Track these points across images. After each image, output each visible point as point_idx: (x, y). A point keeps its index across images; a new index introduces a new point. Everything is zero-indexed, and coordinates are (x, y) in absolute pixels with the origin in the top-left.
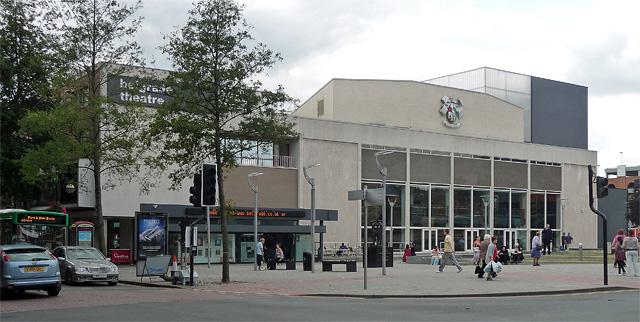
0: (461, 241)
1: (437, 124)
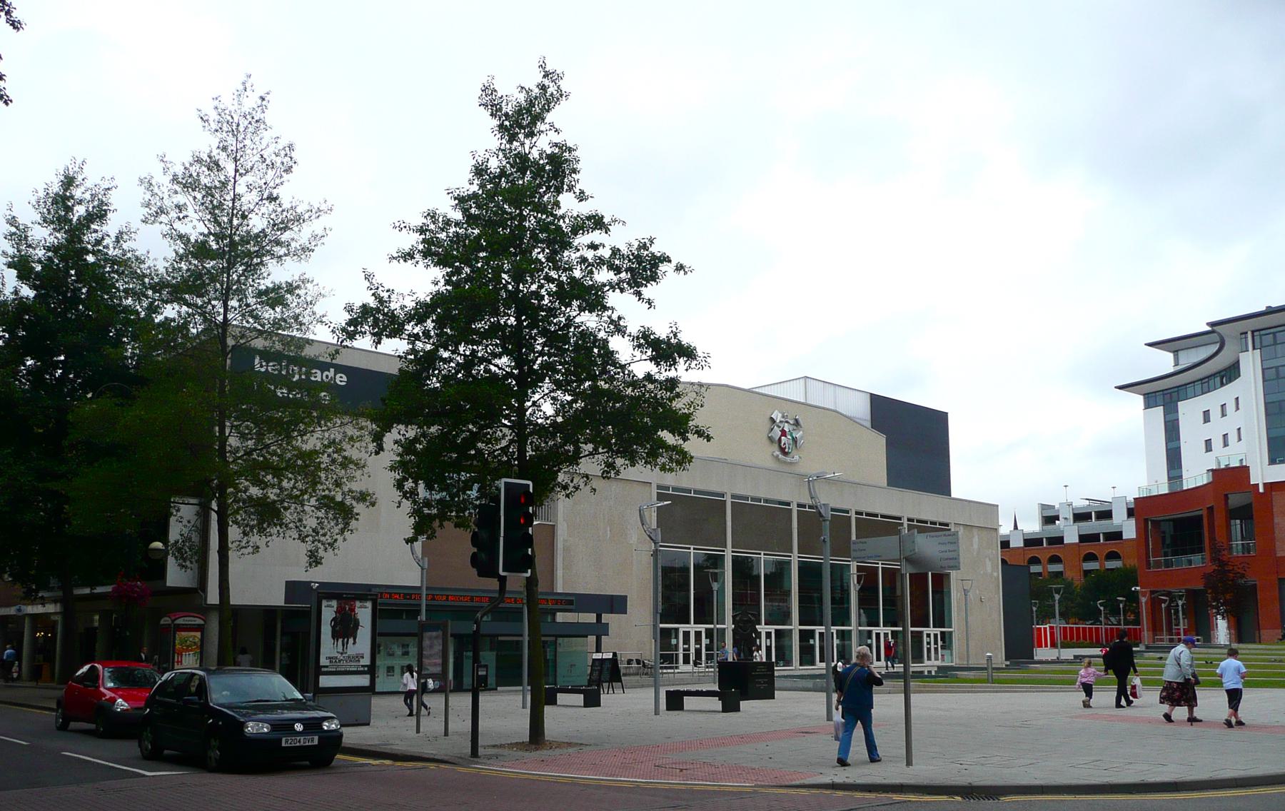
0: (812, 642)
1: (764, 455)
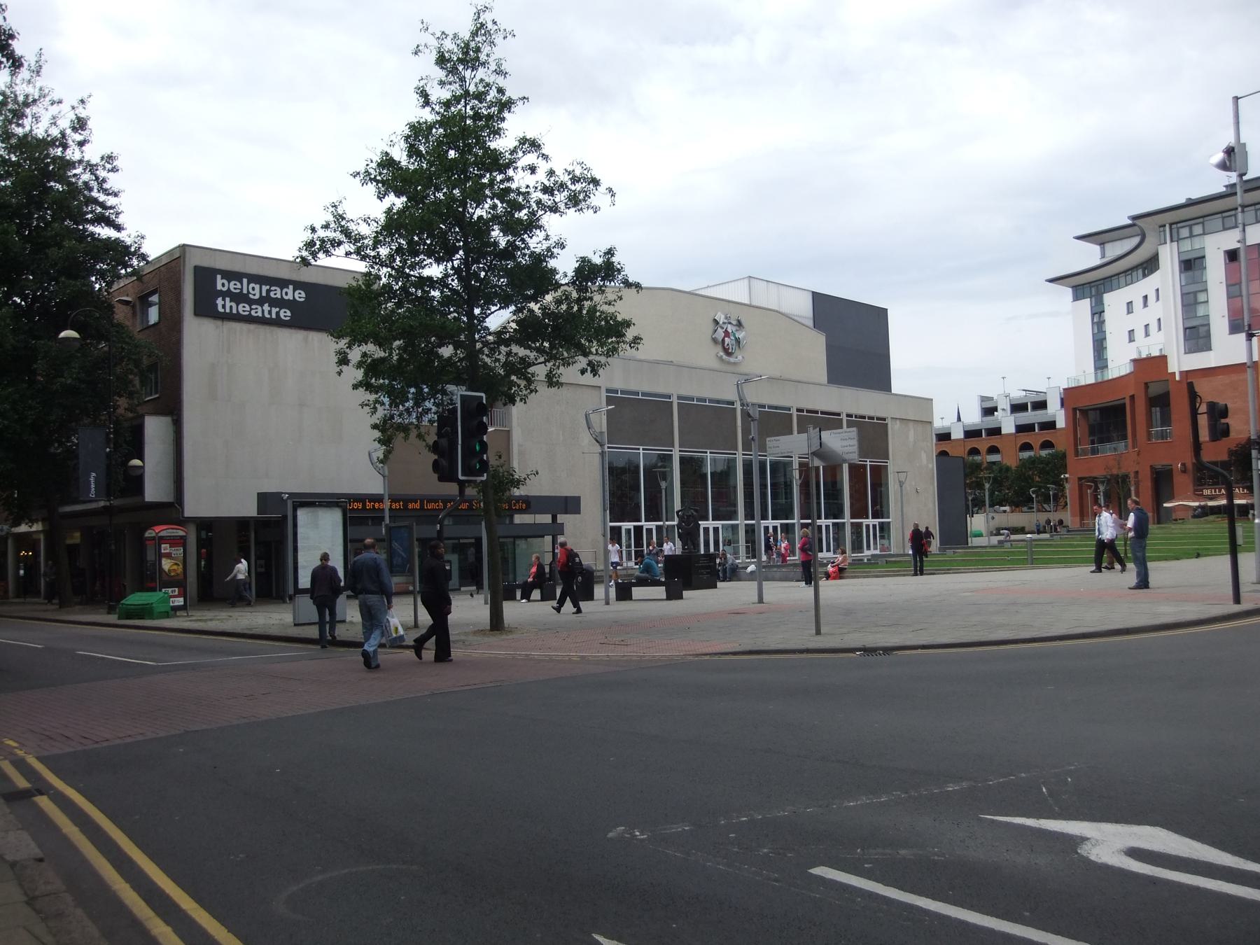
1: (708, 356)
